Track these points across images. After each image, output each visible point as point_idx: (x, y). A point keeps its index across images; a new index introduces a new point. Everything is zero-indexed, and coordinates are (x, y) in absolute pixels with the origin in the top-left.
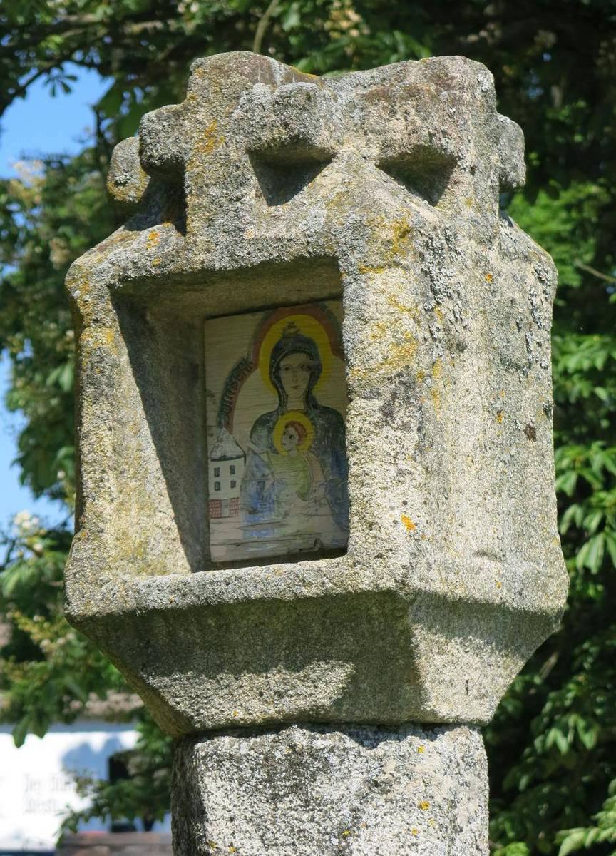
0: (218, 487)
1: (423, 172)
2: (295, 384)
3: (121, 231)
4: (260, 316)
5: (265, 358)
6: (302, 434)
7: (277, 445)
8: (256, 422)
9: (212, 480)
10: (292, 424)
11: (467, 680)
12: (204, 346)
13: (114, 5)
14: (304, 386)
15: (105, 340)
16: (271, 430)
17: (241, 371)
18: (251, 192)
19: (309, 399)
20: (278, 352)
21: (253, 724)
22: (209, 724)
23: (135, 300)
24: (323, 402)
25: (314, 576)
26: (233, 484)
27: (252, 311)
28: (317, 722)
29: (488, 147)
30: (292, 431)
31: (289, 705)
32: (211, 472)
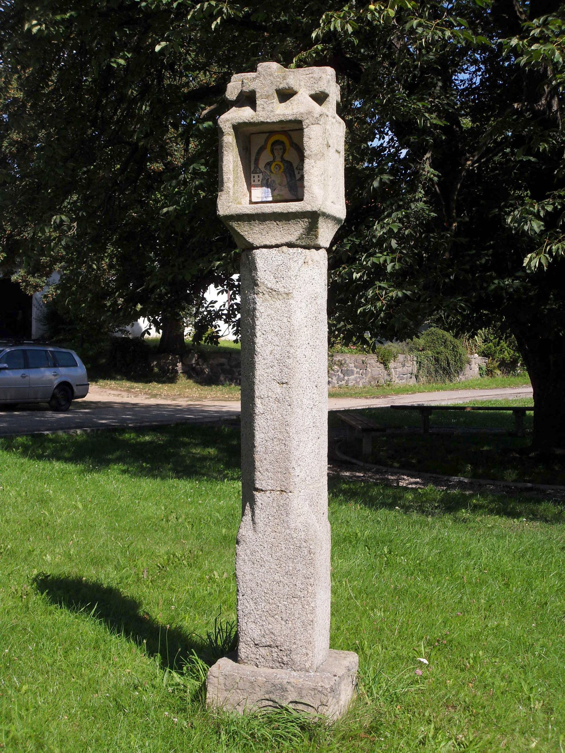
0: (254, 181)
1: (320, 98)
2: (278, 154)
3: (234, 108)
4: (268, 134)
5: (269, 146)
6: (280, 168)
7: (272, 170)
8: (290, 162)
9: (252, 179)
10: (277, 165)
11: (326, 234)
12: (250, 142)
13: (539, 36)
14: (281, 154)
15: (229, 139)
16: (271, 166)
17: (262, 149)
18: (276, 100)
19: (282, 158)
20: (273, 144)
21: (272, 245)
22: (258, 245)
23: (238, 128)
24: (286, 159)
25: (294, 207)
26: (259, 181)
27: (266, 133)
28: (290, 245)
29: (334, 93)
30: (277, 166)
31: (284, 241)
32: (252, 177)
